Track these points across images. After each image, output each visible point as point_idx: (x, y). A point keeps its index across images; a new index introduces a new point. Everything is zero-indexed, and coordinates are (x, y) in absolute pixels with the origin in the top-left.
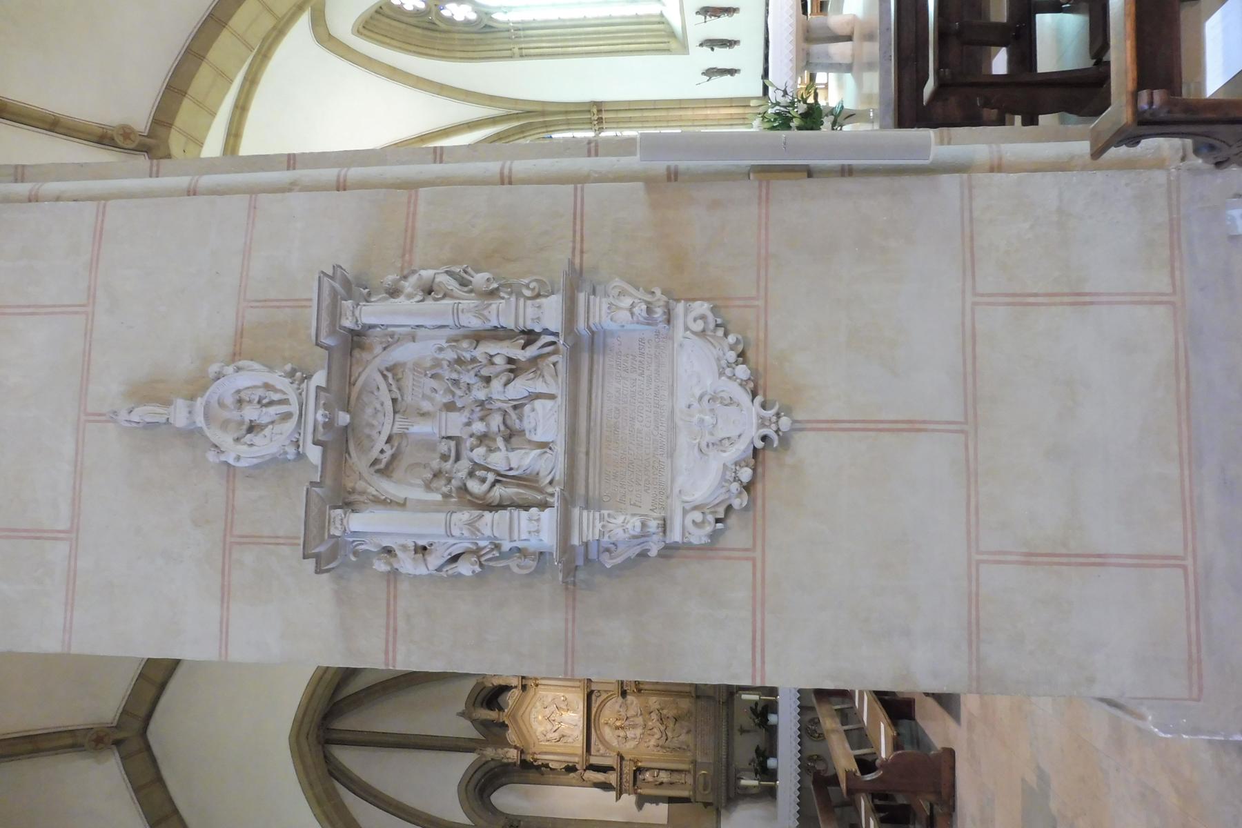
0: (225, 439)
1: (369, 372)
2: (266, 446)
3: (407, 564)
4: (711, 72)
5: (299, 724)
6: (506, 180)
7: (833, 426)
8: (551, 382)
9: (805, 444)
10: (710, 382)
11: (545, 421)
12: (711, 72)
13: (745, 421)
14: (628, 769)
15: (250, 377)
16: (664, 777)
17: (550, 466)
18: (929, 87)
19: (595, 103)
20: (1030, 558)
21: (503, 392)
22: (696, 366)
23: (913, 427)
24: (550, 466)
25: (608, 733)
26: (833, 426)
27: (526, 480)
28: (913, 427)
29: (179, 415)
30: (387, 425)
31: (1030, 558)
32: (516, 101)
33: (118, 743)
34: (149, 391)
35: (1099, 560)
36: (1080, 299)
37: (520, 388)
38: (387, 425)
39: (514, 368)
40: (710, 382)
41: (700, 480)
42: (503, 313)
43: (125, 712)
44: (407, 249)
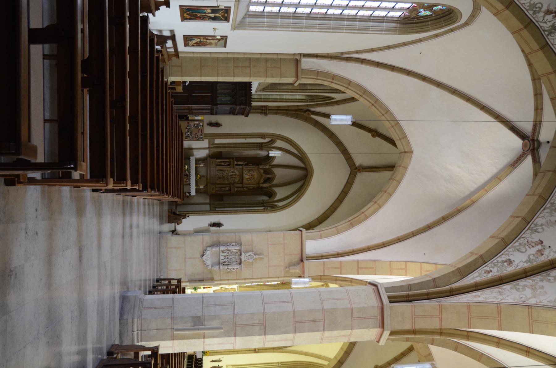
0: (252, 254)
1: (239, 261)
2: (248, 254)
3: (234, 244)
4: (219, 361)
5: (312, 175)
6: (228, 280)
7: (197, 258)
8: (221, 261)
9: (199, 256)
10: (208, 262)
11: (222, 258)
12: (219, 361)
13: (204, 258)
14: (232, 165)
15: (250, 261)
16: (223, 164)
17: (221, 254)
18: (153, 362)
19: (257, 352)
20: (180, 248)
21: (226, 260)
22: (209, 262)
23: (190, 258)
24: (221, 254)
25: (237, 173)
26: (197, 258)
27: (223, 252)
28: (190, 258)
29: (257, 256)
30: (237, 257)
31: (180, 248)
32: (282, 352)
33: (356, 168)
34: (262, 259)
35: (175, 248)
36: (176, 270)
37: (224, 261)
38: (237, 257)
39: (225, 262)
40: (208, 262)
41: (208, 253)
42: (226, 267)
43: (355, 176)
44: (237, 273)
